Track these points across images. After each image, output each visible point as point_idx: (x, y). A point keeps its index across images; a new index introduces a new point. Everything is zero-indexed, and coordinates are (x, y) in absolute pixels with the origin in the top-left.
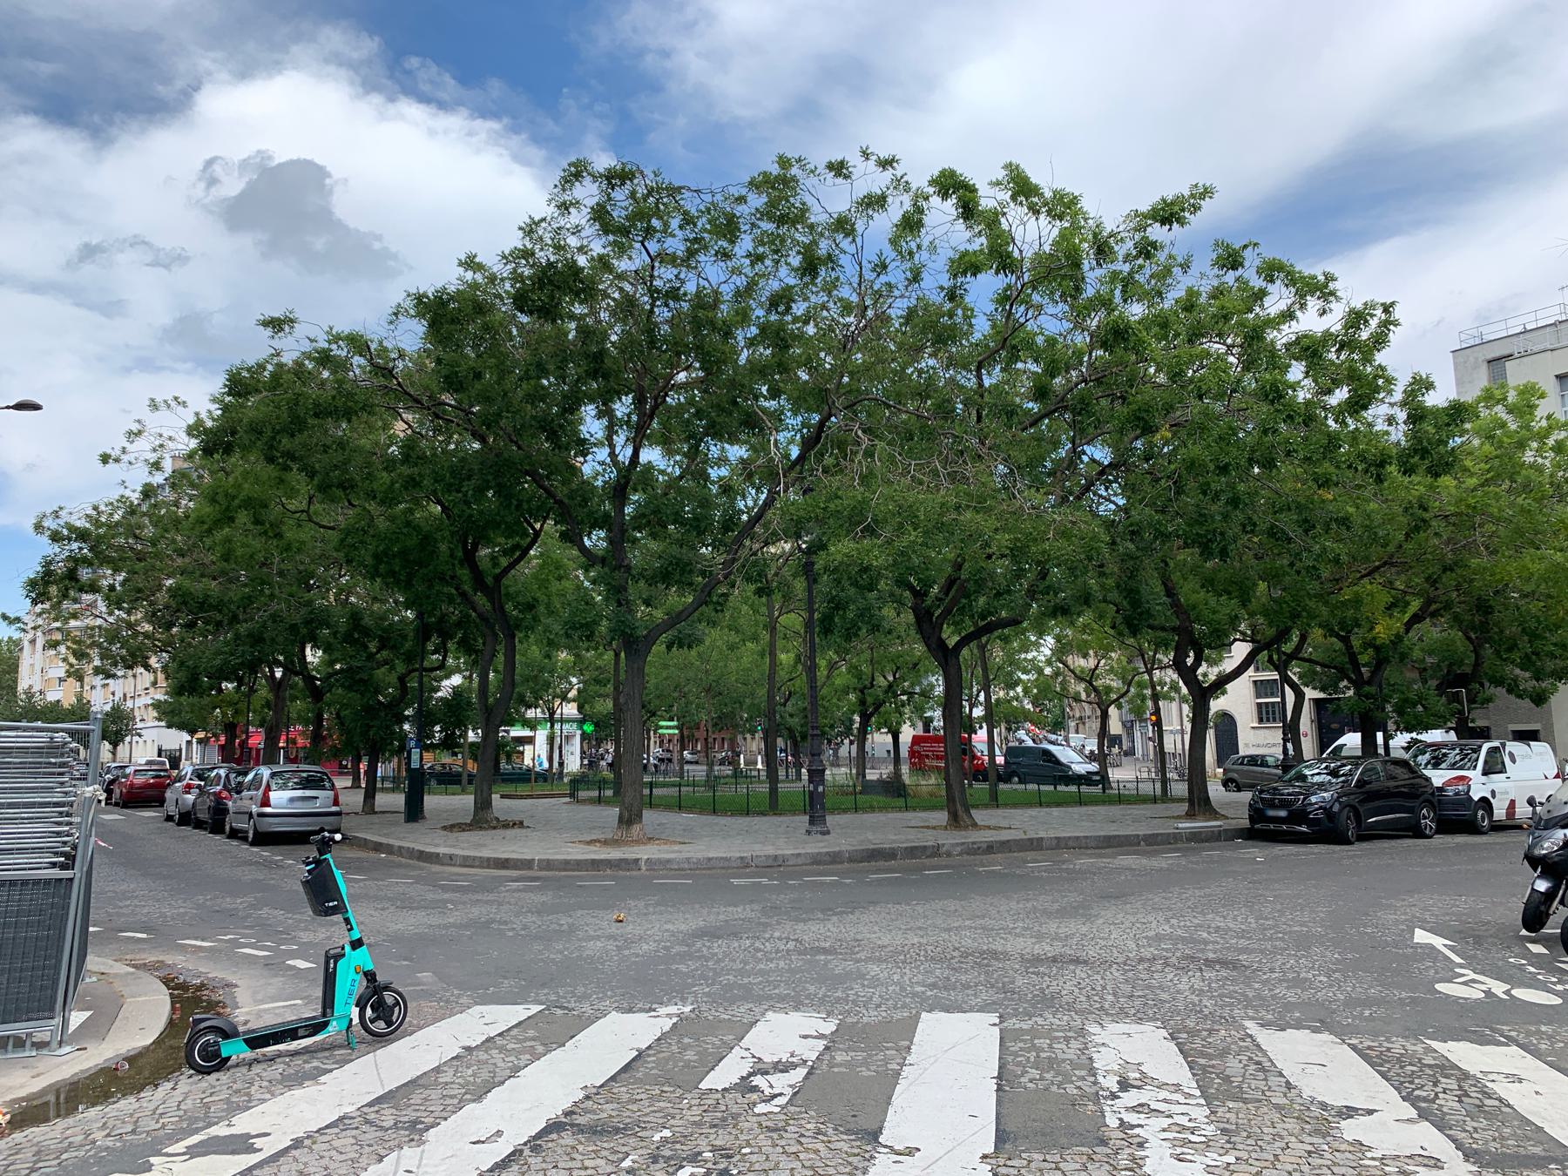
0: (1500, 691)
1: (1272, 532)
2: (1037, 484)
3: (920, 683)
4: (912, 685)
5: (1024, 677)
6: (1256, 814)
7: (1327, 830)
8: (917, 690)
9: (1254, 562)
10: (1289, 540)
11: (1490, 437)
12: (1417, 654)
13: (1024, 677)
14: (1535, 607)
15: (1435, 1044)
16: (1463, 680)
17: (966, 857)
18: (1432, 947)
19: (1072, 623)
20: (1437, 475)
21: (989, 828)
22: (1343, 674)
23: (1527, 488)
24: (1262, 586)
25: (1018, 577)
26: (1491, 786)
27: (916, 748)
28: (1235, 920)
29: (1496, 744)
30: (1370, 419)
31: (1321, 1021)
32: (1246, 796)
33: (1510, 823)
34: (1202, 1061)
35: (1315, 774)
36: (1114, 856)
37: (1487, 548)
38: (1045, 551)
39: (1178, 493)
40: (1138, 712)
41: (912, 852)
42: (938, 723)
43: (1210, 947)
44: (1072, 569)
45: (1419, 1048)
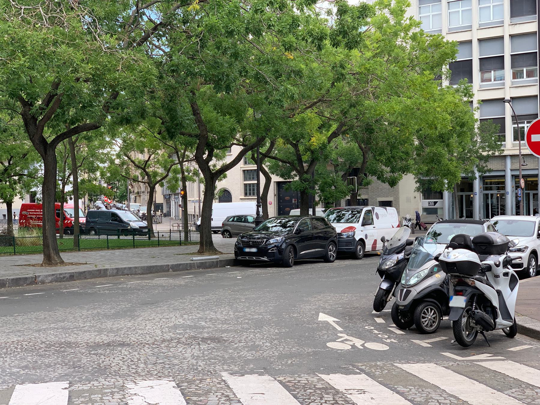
0: (374, 178)
1: (257, 77)
2: (111, 32)
3: (28, 168)
4: (22, 168)
5: (101, 165)
6: (239, 251)
7: (277, 259)
8: (26, 172)
9: (245, 95)
10: (266, 83)
11: (380, 28)
12: (333, 156)
13: (101, 165)
14: (394, 130)
15: (323, 376)
16: (355, 172)
17: (54, 283)
18: (327, 323)
19: (134, 130)
20: (350, 48)
21: (72, 264)
22: (294, 168)
23: (396, 60)
24: (251, 111)
25: (97, 95)
26: (365, 232)
27: (24, 213)
28: (221, 313)
29: (369, 208)
30: (317, 10)
31: (264, 368)
32: (234, 240)
33: (374, 252)
34: (195, 398)
35: (274, 226)
36: (152, 278)
37: (373, 94)
38: (115, 79)
39: (202, 47)
40: (173, 188)
41: (17, 282)
42: (39, 196)
43: (206, 330)
44: (134, 93)
45: (315, 379)
